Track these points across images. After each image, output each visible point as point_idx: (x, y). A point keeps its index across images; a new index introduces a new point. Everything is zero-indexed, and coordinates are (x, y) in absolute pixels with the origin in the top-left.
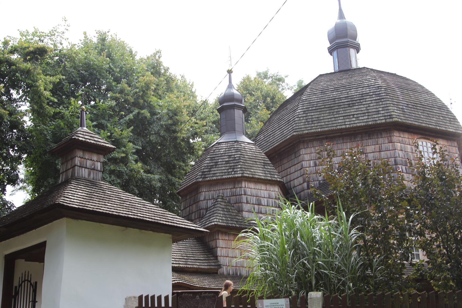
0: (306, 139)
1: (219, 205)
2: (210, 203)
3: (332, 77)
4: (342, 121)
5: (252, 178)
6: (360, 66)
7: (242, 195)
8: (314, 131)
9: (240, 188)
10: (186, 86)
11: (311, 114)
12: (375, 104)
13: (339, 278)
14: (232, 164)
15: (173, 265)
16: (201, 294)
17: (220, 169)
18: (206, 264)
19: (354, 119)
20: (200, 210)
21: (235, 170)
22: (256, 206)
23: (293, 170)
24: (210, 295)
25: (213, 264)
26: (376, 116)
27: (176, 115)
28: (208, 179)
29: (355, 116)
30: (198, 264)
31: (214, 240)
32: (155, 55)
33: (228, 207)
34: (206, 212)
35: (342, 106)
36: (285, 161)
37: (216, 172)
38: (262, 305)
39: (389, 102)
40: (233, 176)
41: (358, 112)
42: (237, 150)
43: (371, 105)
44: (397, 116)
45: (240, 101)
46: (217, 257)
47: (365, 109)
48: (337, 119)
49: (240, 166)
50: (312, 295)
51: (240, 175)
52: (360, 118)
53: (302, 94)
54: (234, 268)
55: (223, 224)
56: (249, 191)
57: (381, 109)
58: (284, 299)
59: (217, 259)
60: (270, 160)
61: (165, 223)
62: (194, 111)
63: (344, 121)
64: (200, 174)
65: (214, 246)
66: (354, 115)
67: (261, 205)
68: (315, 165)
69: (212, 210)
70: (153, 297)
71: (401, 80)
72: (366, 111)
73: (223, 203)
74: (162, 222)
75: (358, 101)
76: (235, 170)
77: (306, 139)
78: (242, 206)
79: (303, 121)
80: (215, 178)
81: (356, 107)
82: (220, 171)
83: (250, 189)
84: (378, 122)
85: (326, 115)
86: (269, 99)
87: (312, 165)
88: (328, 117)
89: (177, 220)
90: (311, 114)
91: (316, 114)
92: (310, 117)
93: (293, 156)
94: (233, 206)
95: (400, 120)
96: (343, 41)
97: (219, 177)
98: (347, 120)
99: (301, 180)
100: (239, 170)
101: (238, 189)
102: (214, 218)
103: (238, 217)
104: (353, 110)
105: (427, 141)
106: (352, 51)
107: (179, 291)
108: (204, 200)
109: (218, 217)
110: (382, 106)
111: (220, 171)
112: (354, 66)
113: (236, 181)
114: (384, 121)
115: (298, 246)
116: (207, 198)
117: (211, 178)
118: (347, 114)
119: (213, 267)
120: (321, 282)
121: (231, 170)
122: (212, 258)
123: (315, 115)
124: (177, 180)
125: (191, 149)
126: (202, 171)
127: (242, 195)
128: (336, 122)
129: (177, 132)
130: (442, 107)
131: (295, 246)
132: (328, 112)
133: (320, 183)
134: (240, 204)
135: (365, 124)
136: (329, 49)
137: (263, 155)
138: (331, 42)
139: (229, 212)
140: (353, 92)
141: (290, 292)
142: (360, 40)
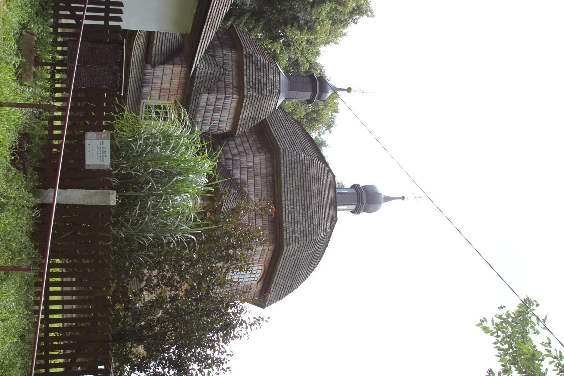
0: (275, 161)
1: (217, 70)
2: (219, 60)
3: (332, 188)
4: (289, 197)
5: (242, 106)
6: (339, 213)
7: (225, 94)
8: (282, 169)
9: (233, 93)
10: (336, 37)
11: (299, 167)
12: (302, 230)
13: (131, 221)
14: (257, 87)
15: (156, 33)
16: (120, 72)
17: (254, 73)
18: (157, 52)
19: (290, 209)
20: (214, 49)
21: (251, 89)
22: (213, 107)
23: (246, 144)
24: (118, 82)
25: (156, 60)
26: (290, 230)
27: (309, 28)
28: (245, 61)
29: (293, 210)
30: (157, 44)
31: (181, 62)
32: (372, 13)
33: (214, 79)
34: (211, 55)
35: (303, 198)
36: (255, 137)
37: (251, 69)
38: (105, 138)
39: (302, 243)
40: (246, 87)
41: (296, 213)
42: (271, 92)
43: (302, 226)
44: (288, 250)
45: (319, 98)
46: (164, 64)
47: (299, 220)
48: (292, 192)
49: (254, 94)
50: (113, 195)
51: (245, 94)
52: (290, 215)
53: (319, 159)
54: (151, 81)
55: (197, 73)
56: (228, 101)
57: (296, 235)
58: (110, 163)
59: (161, 64)
60: (257, 124)
61: (204, 30)
62: (311, 43)
63: (289, 199)
64: (251, 52)
65: (175, 62)
66: (294, 209)
67: (213, 112)
68: (248, 168)
69: (212, 62)
70: (120, 12)
71: (321, 253)
72: (296, 221)
73: (218, 74)
74: (205, 27)
75: (306, 214)
76: (251, 89)
77: (275, 161)
78: (214, 93)
79: (293, 159)
80: (245, 67)
81: (301, 211)
82: (251, 73)
83: (231, 103)
84: (285, 232)
85: (297, 182)
86: (314, 118)
87: (249, 164)
88: (294, 184)
89: (206, 42)
90: (299, 167)
91: (299, 172)
92: (296, 166)
93: (259, 145)
94: (214, 84)
95: (284, 252)
96: (364, 199)
97: (245, 72)
98: (289, 203)
99: (235, 152)
100: (251, 93)
101: (231, 91)
102: (204, 64)
103: (203, 88)
104: (298, 209)
105: (261, 274)
106: (353, 207)
107: (124, 47)
108: (223, 54)
109: (204, 69)
110: (299, 236)
111: (251, 73)
112: (339, 207)
113: (240, 89)
114: (285, 237)
115: (169, 177)
116: (225, 57)
117: (245, 64)
118: (295, 202)
119: (153, 59)
120: (126, 203)
121: (251, 85)
122: (162, 58)
123: (298, 171)
124: (244, 21)
125: (275, 38)
126: (254, 55)
127: (225, 94)
128: (289, 192)
129: (291, 27)
130: (291, 288)
131: (169, 174)
132: (299, 184)
133: (230, 170)
134: (216, 91)
135: (284, 219)
136: (358, 185)
137: (263, 118)
138: (364, 187)
139: (209, 80)
140: (315, 209)
141: (117, 168)
142: (363, 215)
